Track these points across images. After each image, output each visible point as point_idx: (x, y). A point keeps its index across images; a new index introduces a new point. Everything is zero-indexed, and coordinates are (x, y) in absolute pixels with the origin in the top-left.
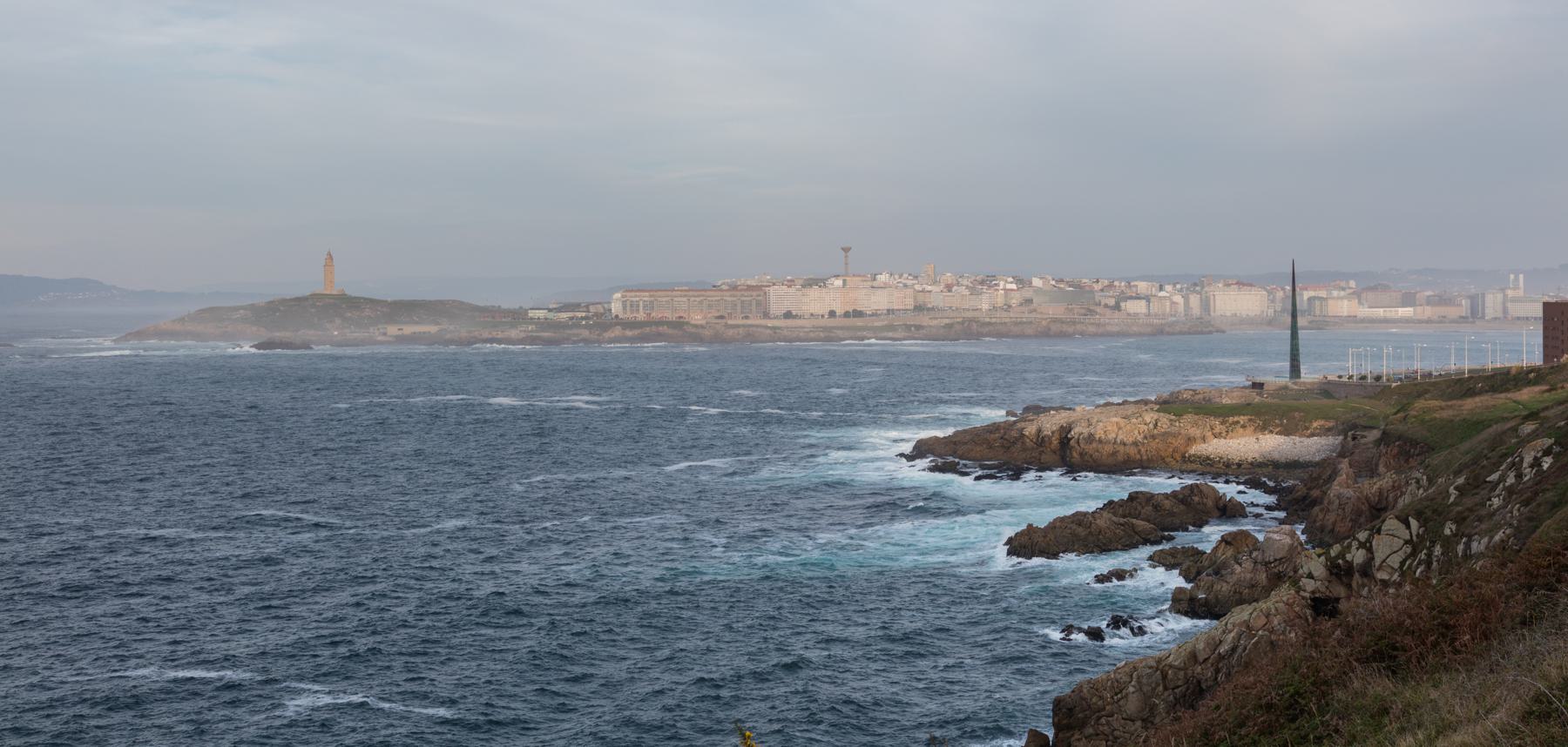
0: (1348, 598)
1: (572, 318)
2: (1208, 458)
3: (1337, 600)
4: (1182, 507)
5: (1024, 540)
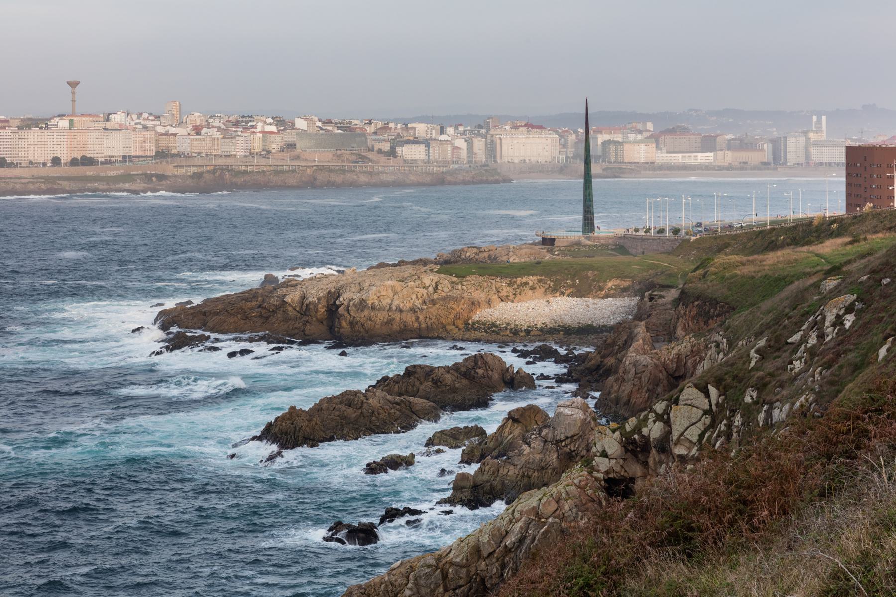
2: (494, 325)
3: (632, 480)
4: (465, 381)
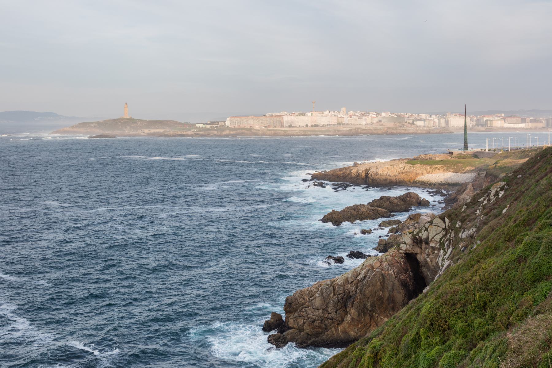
0: (421, 253)
1: (211, 127)
2: (423, 182)
3: (416, 254)
4: (402, 202)
5: (326, 218)
